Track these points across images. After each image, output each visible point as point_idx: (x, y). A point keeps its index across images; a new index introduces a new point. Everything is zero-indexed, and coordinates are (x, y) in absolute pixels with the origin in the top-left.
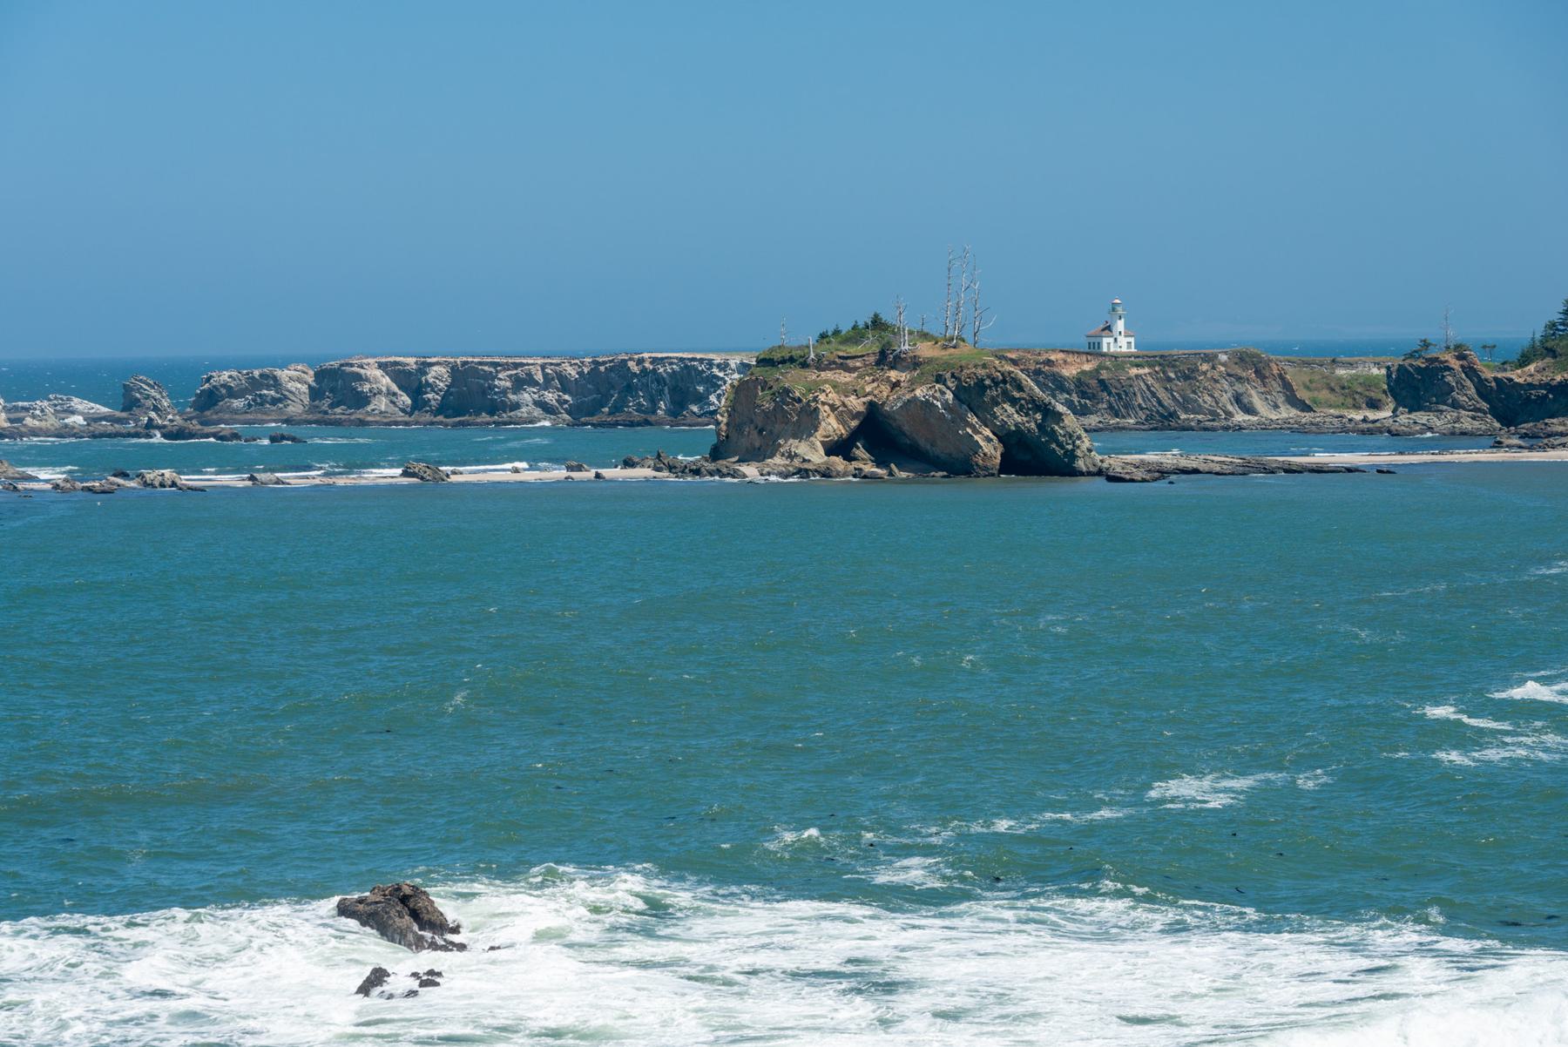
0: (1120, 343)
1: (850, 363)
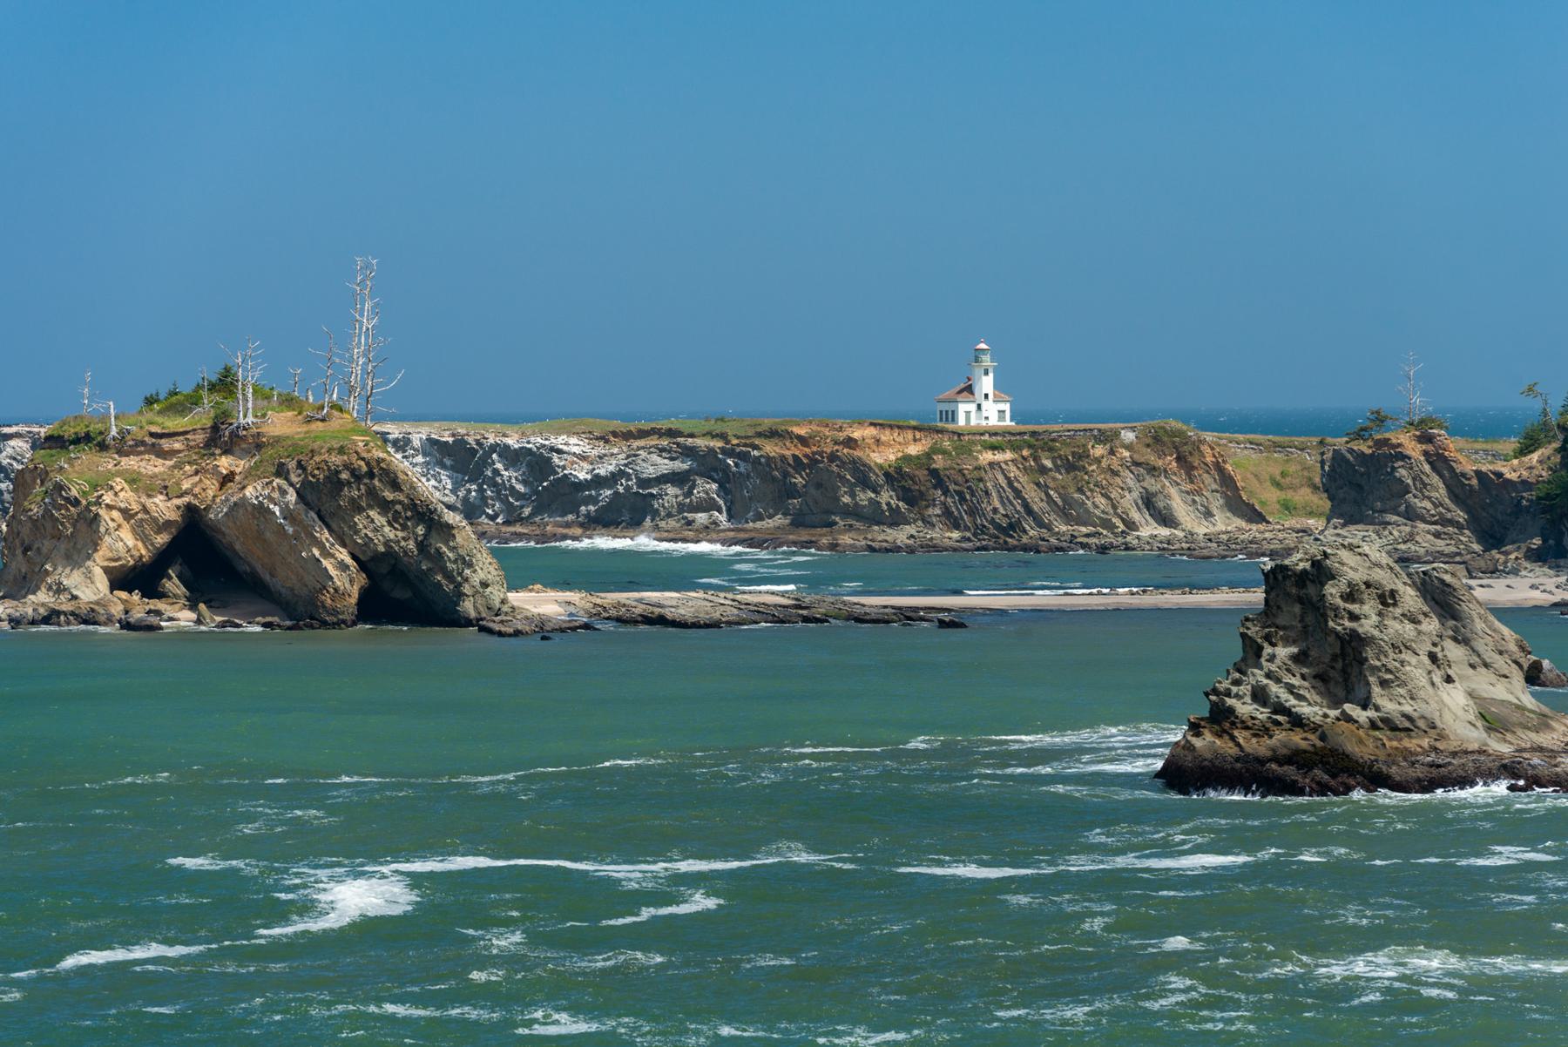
0: (987, 410)
1: (166, 444)
